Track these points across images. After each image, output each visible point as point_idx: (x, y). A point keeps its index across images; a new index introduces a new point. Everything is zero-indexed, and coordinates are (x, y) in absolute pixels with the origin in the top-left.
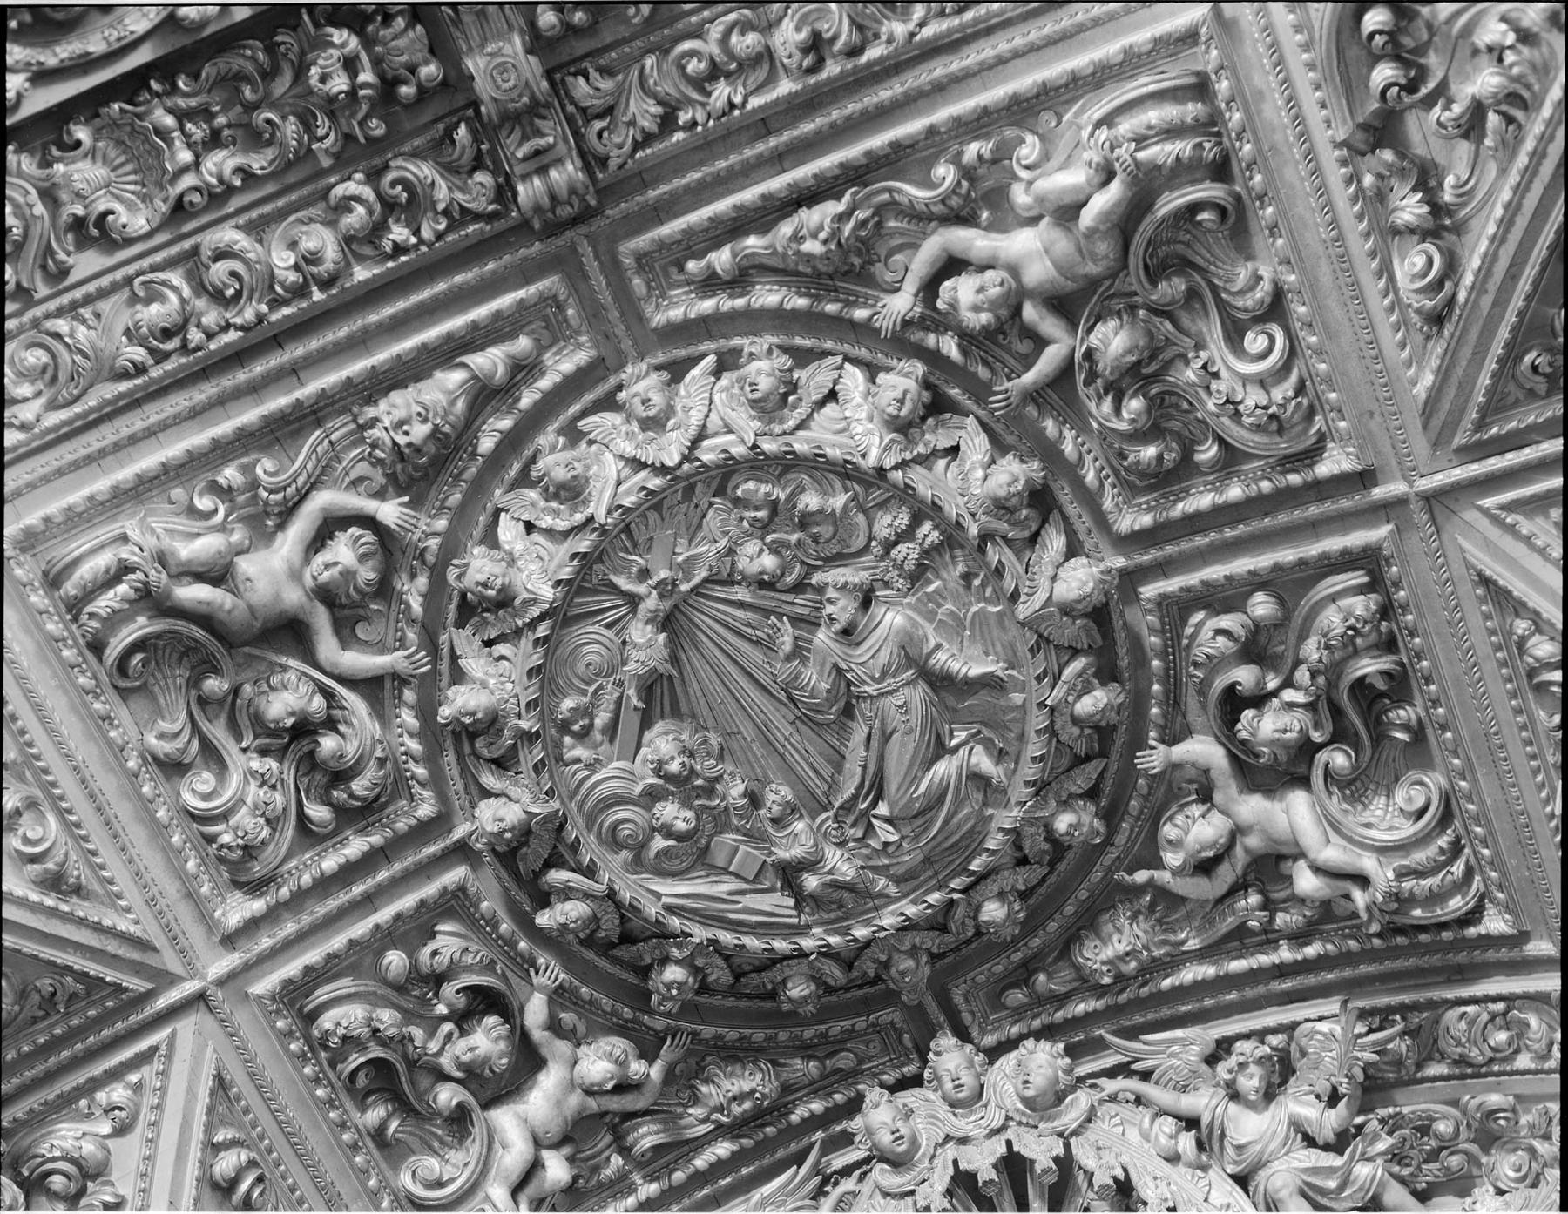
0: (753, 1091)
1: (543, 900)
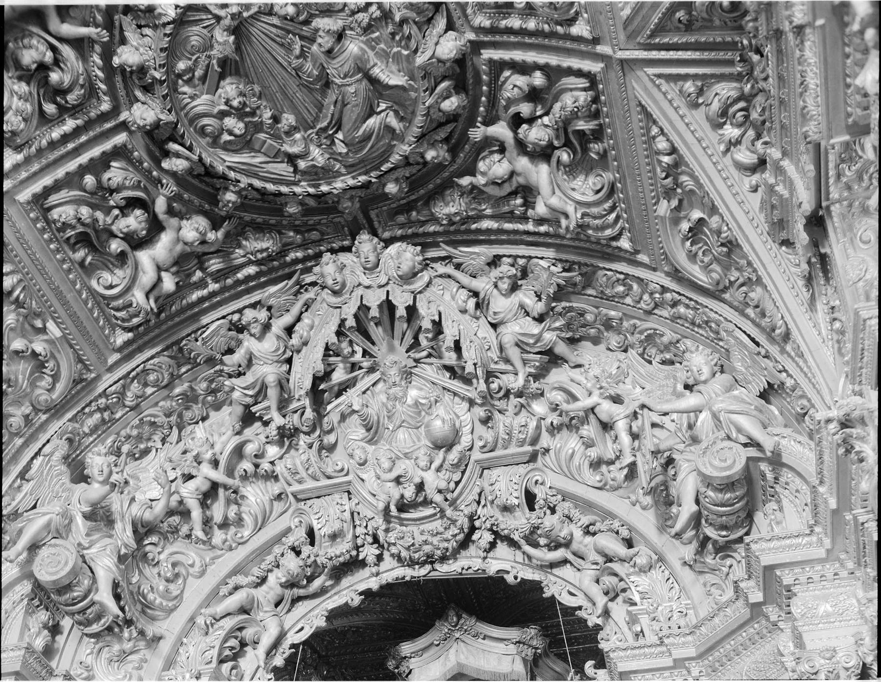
0: (268, 248)
1: (167, 154)
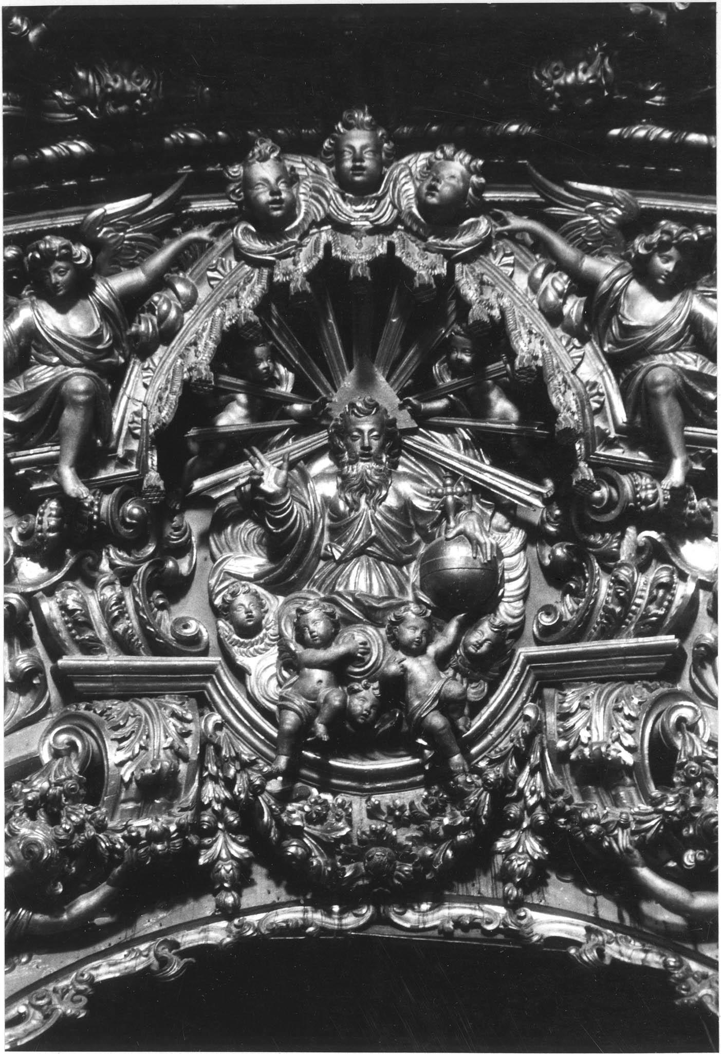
0: (136, 95)
